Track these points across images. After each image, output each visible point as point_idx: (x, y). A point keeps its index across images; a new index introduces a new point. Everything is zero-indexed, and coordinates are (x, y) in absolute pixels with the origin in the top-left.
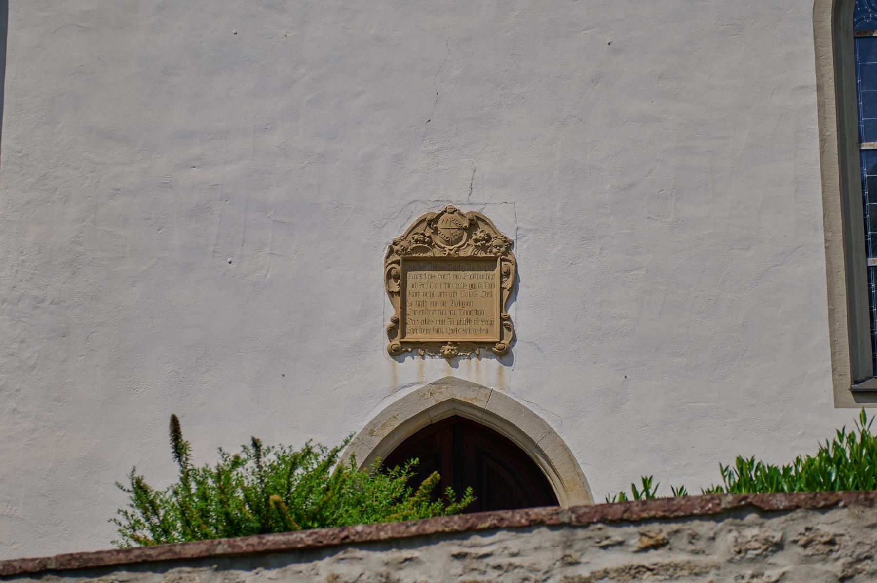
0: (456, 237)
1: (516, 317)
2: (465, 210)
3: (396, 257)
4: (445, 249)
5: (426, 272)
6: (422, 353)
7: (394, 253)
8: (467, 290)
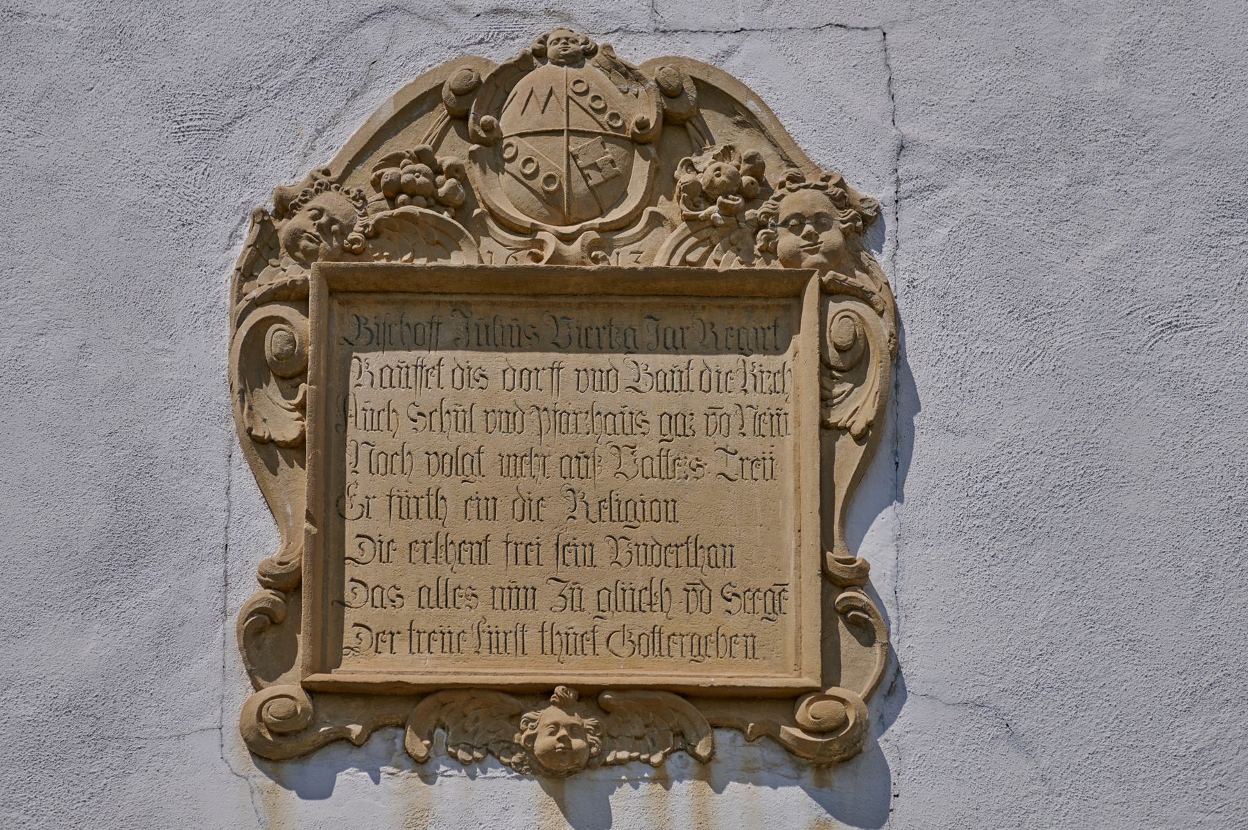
0: (596, 178)
1: (897, 576)
2: (634, 53)
3: (288, 271)
4: (540, 235)
5: (439, 354)
6: (419, 747)
7: (283, 250)
8: (649, 445)
